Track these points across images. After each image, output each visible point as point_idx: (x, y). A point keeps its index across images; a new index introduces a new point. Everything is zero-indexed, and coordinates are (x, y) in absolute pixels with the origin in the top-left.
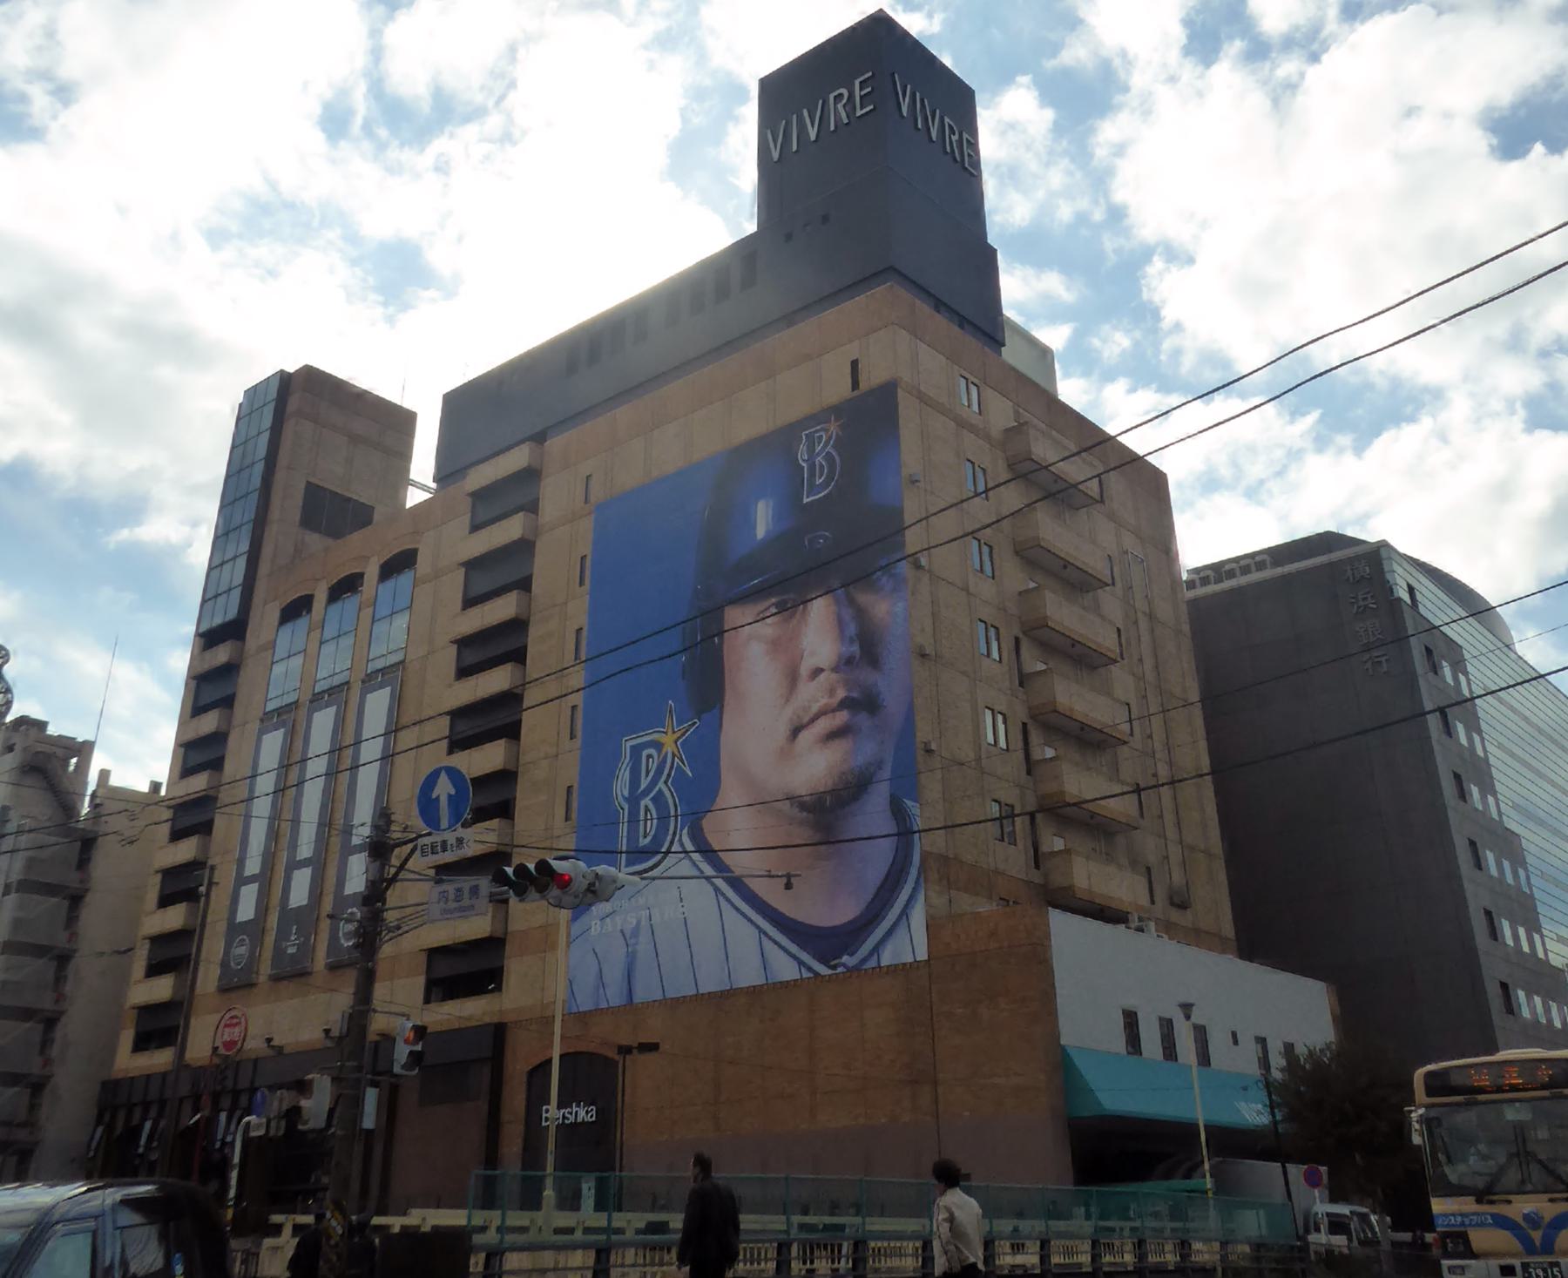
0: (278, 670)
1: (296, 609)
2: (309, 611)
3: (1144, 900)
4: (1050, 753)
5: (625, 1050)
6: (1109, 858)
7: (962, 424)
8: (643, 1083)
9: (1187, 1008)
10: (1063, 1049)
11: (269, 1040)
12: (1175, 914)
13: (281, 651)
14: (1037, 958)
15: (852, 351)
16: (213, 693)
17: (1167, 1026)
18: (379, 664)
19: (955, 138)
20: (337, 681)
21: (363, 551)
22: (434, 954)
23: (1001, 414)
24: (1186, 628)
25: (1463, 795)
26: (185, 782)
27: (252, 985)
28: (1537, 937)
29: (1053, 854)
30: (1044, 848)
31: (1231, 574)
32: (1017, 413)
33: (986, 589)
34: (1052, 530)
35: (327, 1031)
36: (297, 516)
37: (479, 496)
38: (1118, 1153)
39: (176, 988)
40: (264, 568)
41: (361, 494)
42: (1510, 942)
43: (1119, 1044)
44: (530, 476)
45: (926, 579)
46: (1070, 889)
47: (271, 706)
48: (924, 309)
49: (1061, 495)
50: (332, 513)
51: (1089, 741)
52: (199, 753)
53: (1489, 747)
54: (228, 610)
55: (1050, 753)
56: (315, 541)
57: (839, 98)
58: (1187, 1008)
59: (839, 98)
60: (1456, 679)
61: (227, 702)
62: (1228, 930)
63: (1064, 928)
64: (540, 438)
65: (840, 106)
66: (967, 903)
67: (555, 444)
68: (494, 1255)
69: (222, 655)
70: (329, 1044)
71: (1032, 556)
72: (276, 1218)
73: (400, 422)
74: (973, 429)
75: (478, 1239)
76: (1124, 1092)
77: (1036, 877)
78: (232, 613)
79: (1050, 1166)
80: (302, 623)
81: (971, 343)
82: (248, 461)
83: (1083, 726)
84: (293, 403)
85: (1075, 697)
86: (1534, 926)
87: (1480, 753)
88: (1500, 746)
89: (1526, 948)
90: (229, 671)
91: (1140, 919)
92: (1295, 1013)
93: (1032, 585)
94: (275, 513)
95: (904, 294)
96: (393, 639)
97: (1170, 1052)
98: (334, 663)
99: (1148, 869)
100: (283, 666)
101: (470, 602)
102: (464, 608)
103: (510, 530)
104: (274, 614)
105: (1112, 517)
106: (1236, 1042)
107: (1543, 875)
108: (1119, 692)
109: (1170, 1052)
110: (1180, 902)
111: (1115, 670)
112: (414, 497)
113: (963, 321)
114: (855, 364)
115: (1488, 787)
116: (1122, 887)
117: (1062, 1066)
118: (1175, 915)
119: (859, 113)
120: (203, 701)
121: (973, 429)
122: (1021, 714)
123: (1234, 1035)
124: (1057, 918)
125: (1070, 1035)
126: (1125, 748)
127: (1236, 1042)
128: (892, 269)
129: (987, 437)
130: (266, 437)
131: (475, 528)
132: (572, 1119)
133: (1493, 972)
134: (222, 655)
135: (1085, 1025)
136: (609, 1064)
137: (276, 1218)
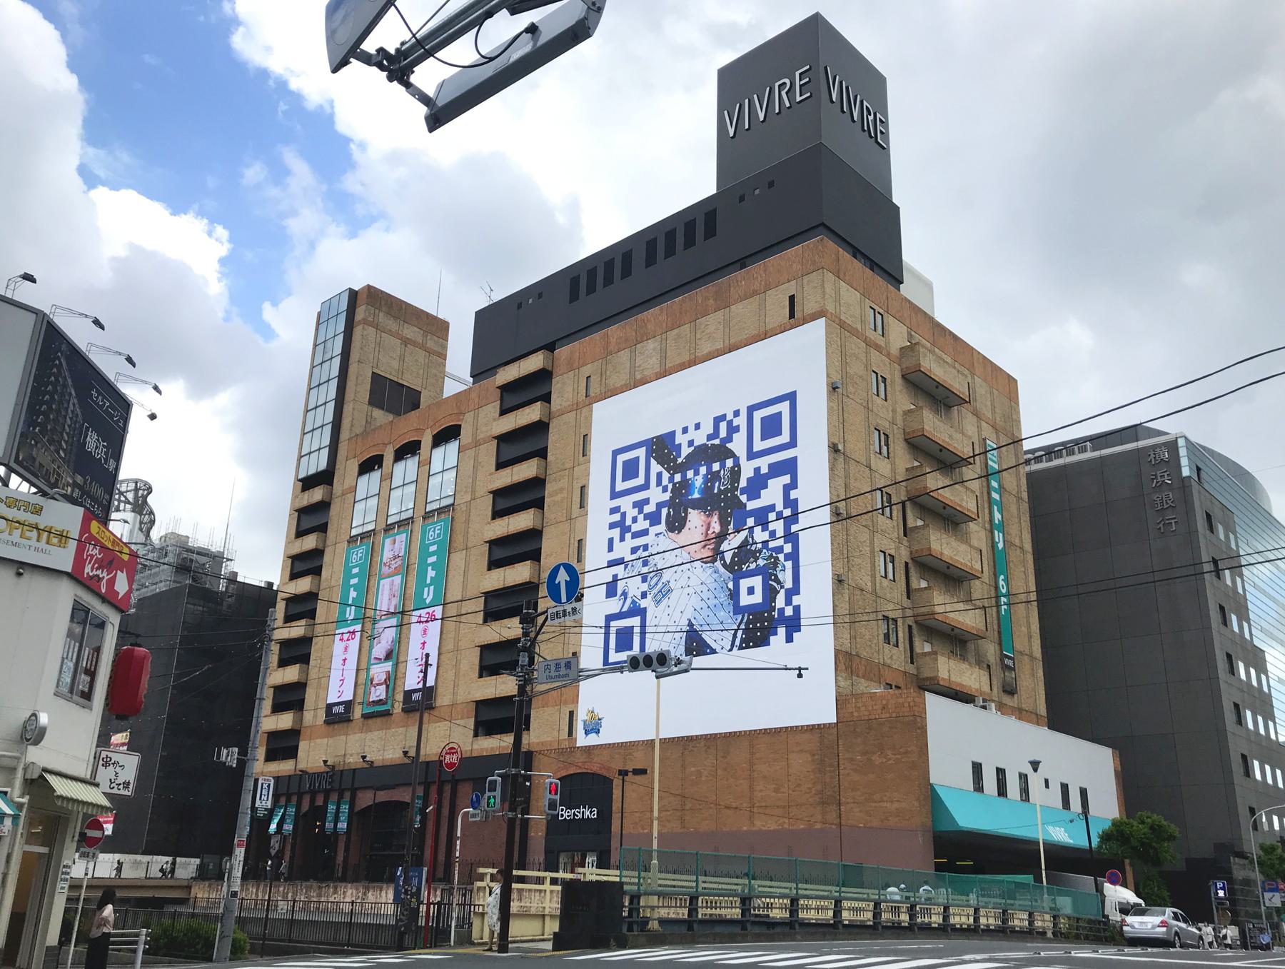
0: (359, 507)
1: (369, 465)
2: (380, 466)
3: (986, 688)
4: (924, 584)
5: (623, 773)
6: (964, 658)
7: (869, 344)
8: (627, 797)
9: (1035, 765)
10: (931, 785)
11: (364, 757)
12: (1006, 695)
13: (360, 494)
14: (917, 727)
15: (791, 288)
16: (309, 522)
17: (1023, 778)
18: (435, 506)
19: (871, 118)
20: (404, 516)
21: (419, 425)
22: (480, 704)
23: (898, 336)
24: (1025, 495)
25: (1225, 622)
26: (293, 583)
27: (349, 720)
28: (1271, 724)
29: (925, 654)
30: (918, 650)
31: (1058, 454)
32: (910, 335)
33: (883, 467)
34: (934, 425)
35: (405, 753)
36: (366, 397)
37: (506, 389)
38: (973, 856)
39: (294, 721)
40: (345, 435)
41: (409, 380)
42: (1251, 726)
43: (969, 784)
44: (543, 376)
45: (841, 459)
46: (935, 679)
47: (354, 532)
48: (845, 256)
49: (941, 399)
50: (394, 396)
51: (952, 578)
52: (304, 564)
53: (1247, 586)
54: (319, 463)
55: (924, 584)
56: (380, 416)
57: (782, 86)
58: (1035, 765)
59: (782, 86)
60: (1227, 537)
61: (323, 528)
62: (1042, 710)
63: (935, 706)
64: (551, 347)
65: (783, 93)
66: (863, 686)
67: (563, 352)
68: (635, 898)
69: (317, 494)
70: (407, 761)
71: (921, 447)
72: (481, 870)
73: (439, 328)
74: (878, 348)
75: (626, 887)
76: (973, 814)
77: (911, 669)
78: (323, 465)
79: (921, 856)
80: (376, 475)
81: (879, 281)
82: (328, 356)
83: (949, 566)
84: (360, 313)
85: (944, 546)
86: (1269, 715)
87: (1240, 591)
88: (1255, 586)
89: (1262, 731)
90: (324, 506)
91: (984, 701)
92: (1090, 767)
93: (916, 464)
94: (349, 395)
95: (830, 245)
96: (442, 487)
97: (1002, 791)
98: (402, 503)
99: (989, 666)
100: (363, 503)
101: (500, 465)
102: (497, 469)
103: (531, 414)
104: (354, 467)
105: (976, 413)
106: (1047, 786)
107: (1255, 586)
108: (975, 543)
109: (1002, 791)
110: (1010, 690)
111: (972, 526)
112: (451, 388)
113: (873, 265)
114: (792, 298)
115: (1244, 615)
116: (969, 677)
117: (932, 798)
118: (1006, 699)
119: (798, 99)
120: (305, 526)
121: (878, 348)
122: (904, 555)
123: (1047, 781)
124: (930, 698)
125: (937, 776)
126: (977, 582)
127: (1047, 786)
128: (823, 224)
129: (888, 355)
130: (341, 338)
131: (503, 412)
132: (580, 816)
133: (1236, 747)
134: (317, 494)
135: (947, 770)
136: (606, 783)
137: (481, 870)
